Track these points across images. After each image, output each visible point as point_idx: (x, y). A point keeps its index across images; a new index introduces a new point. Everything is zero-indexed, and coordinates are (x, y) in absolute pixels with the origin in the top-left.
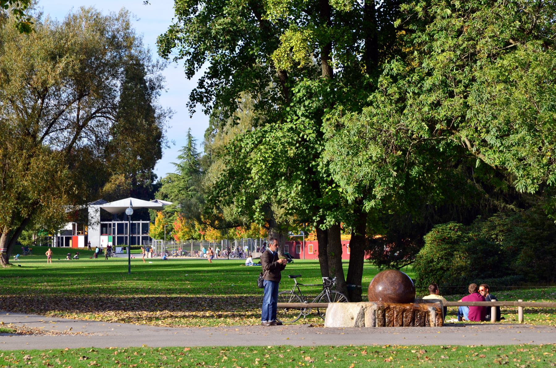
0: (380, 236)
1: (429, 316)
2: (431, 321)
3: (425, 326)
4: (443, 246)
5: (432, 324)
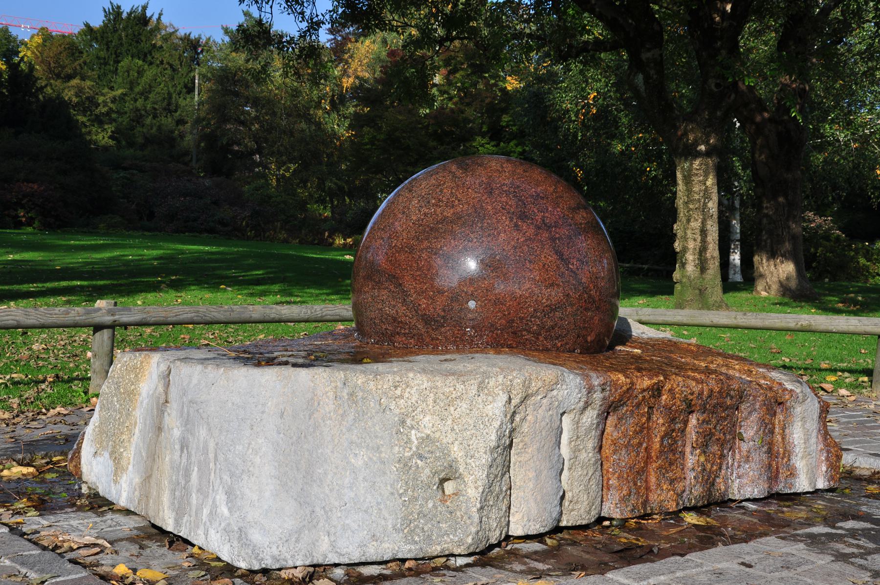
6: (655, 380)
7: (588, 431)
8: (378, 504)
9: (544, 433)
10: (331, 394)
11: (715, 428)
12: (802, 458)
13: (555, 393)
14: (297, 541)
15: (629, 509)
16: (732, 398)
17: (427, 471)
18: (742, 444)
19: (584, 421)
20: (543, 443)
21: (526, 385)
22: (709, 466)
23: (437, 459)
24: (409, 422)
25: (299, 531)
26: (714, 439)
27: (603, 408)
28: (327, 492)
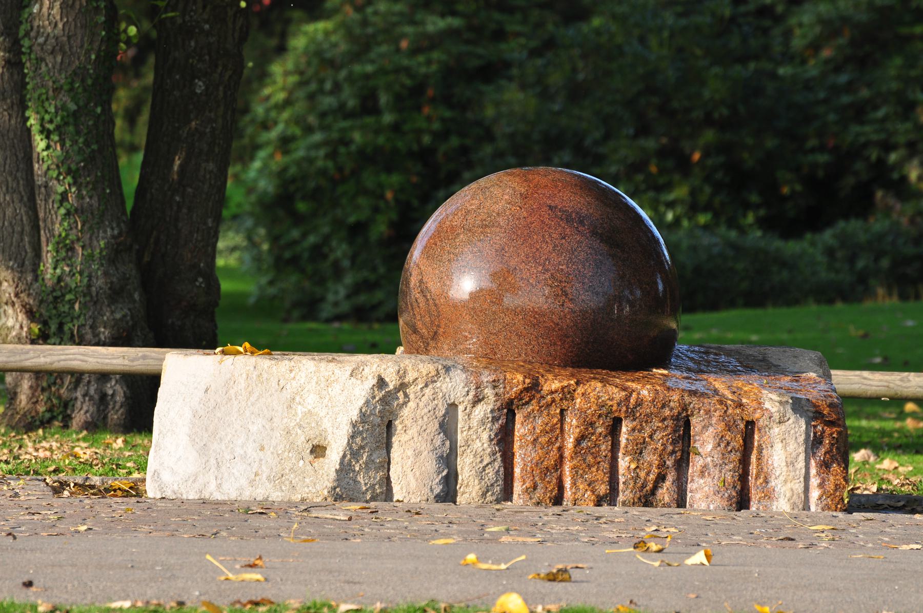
6: (565, 383)
7: (483, 422)
8: (261, 460)
9: (425, 418)
10: (244, 376)
11: (651, 437)
12: (785, 481)
13: (438, 384)
14: (194, 481)
15: (534, 501)
16: (672, 409)
17: (303, 438)
18: (697, 458)
19: (477, 412)
20: (424, 427)
21: (401, 373)
22: (642, 474)
23: (312, 428)
24: (298, 399)
25: (196, 476)
26: (650, 447)
27: (499, 404)
28: (223, 448)
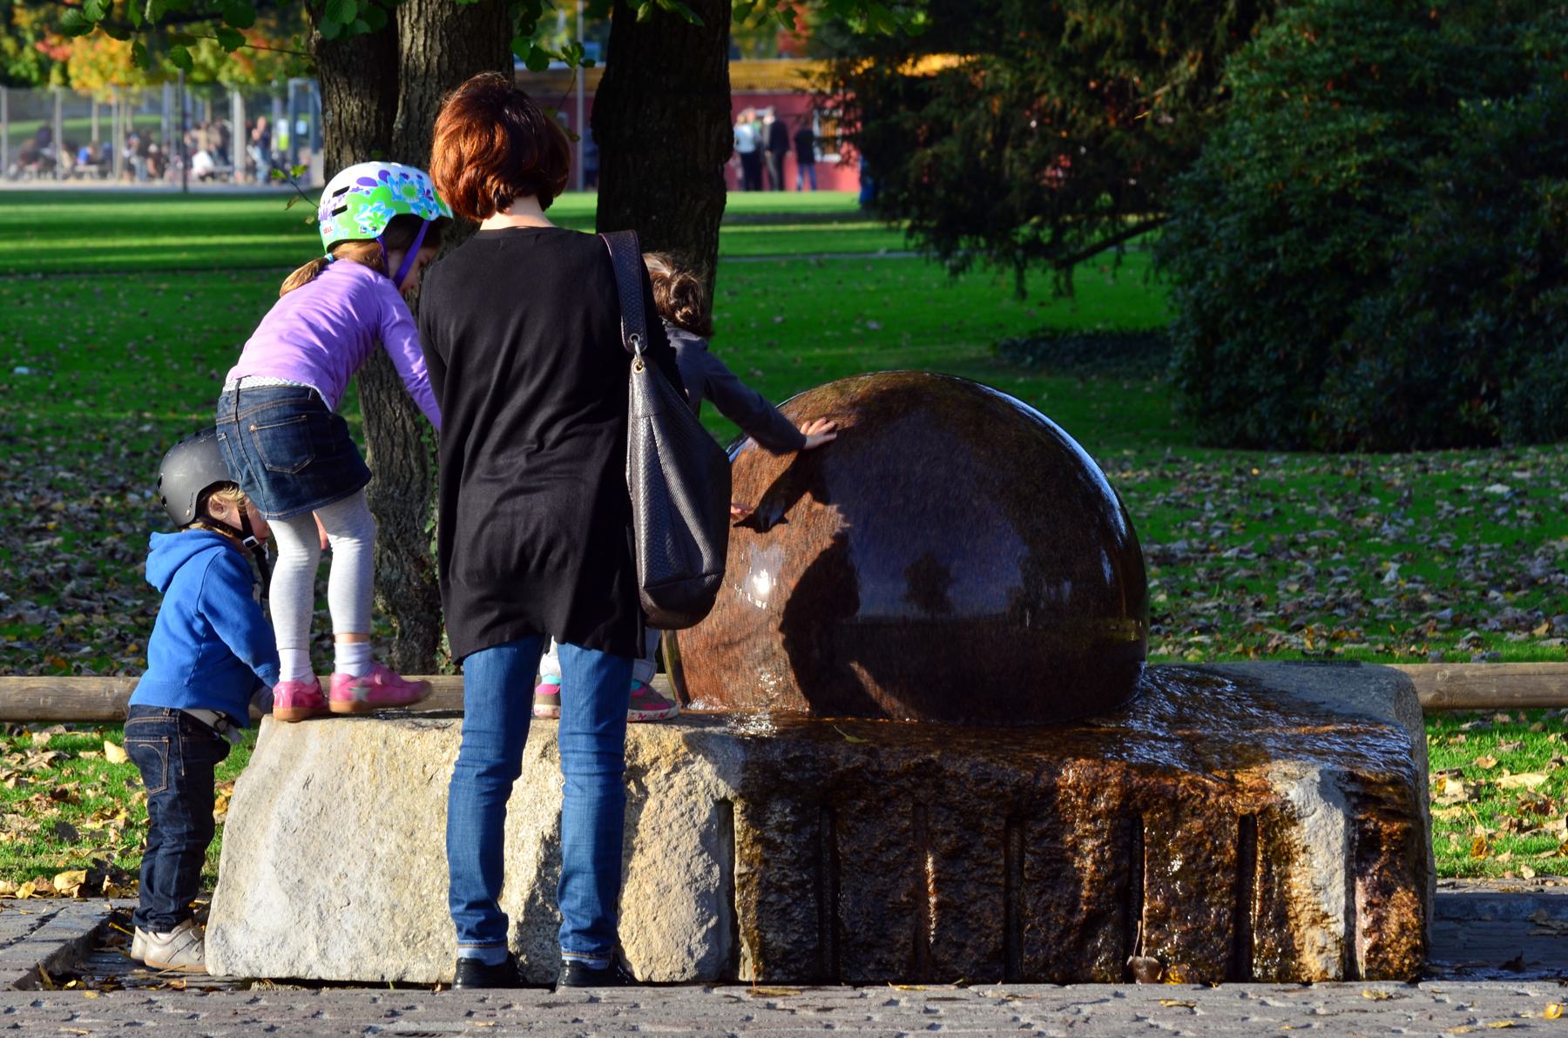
0: (952, 61)
1: (1283, 856)
2: (1302, 911)
3: (1238, 971)
4: (1354, 121)
5: (1315, 951)
14: (282, 945)
20: (675, 843)
